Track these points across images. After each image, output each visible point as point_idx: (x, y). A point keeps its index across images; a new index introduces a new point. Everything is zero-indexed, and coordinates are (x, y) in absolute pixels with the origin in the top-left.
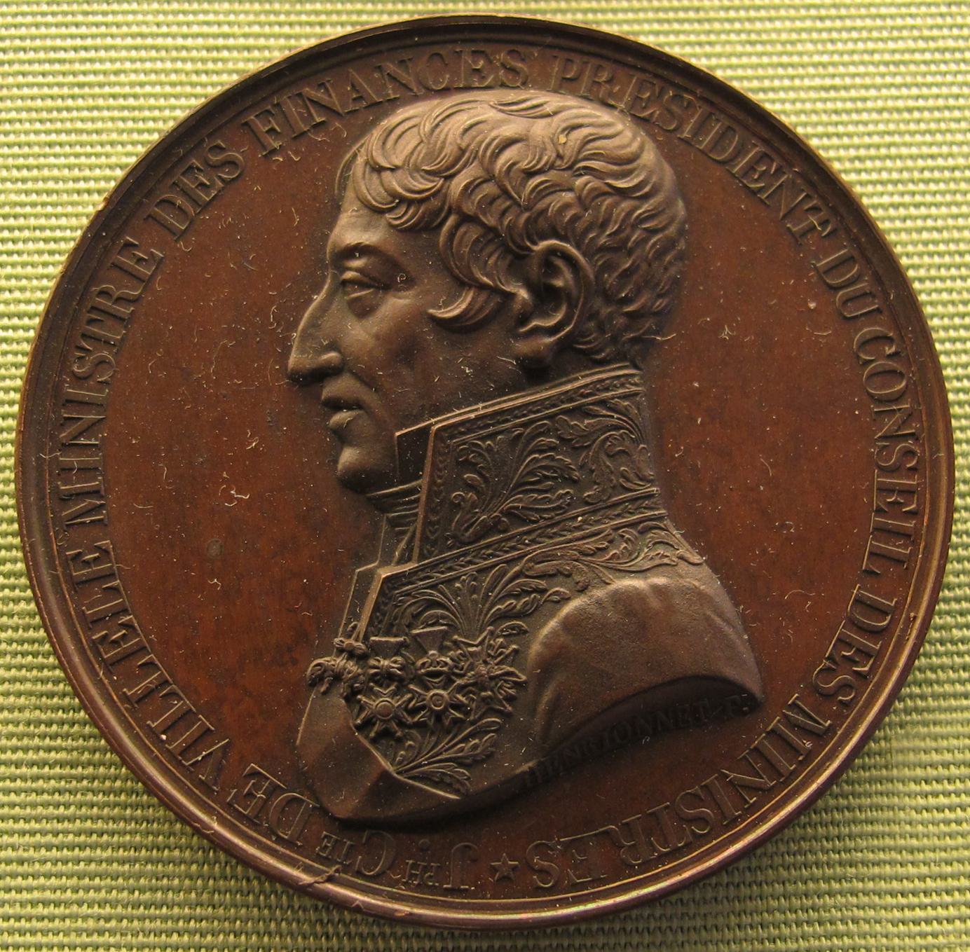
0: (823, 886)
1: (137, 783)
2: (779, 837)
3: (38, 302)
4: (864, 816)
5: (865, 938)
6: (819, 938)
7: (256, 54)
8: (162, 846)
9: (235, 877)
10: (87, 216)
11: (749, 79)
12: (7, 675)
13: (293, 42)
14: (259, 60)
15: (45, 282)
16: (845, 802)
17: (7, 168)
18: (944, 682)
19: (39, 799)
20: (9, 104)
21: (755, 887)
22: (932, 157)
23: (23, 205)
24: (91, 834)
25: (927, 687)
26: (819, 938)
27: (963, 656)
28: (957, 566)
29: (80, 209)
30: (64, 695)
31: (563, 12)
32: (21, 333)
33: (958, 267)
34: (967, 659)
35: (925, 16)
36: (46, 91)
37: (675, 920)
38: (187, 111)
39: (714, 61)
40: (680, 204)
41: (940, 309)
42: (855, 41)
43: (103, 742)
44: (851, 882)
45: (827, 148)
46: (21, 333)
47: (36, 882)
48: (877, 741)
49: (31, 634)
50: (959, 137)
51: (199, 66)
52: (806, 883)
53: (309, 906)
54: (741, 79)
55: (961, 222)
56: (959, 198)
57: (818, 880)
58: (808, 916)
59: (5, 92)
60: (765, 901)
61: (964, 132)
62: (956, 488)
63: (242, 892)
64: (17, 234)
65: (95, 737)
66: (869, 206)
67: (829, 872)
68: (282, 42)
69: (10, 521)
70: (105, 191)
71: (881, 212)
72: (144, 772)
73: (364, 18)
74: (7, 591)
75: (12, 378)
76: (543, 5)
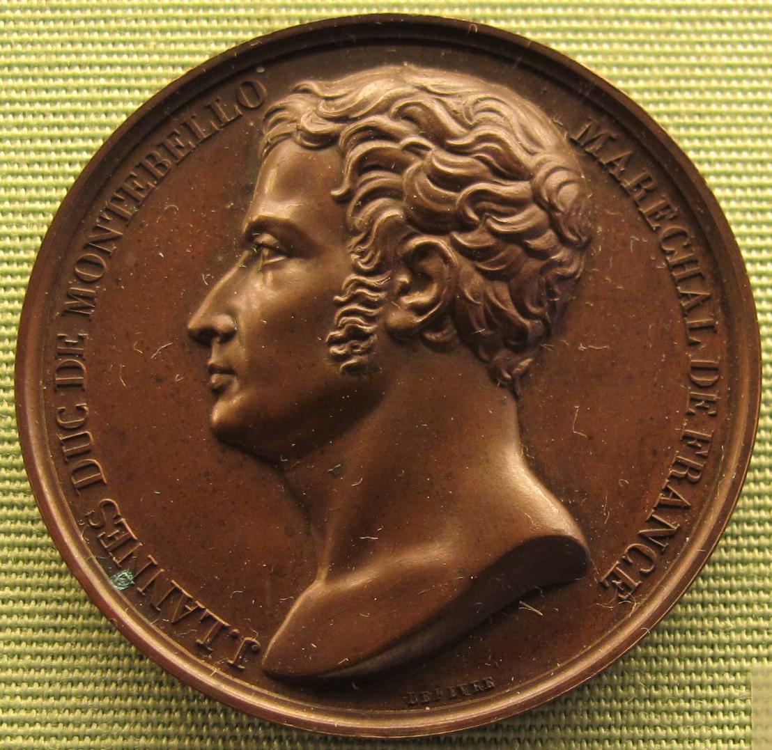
1: (130, 646)
4: (706, 584)
9: (216, 724)
10: (81, 163)
12: (7, 539)
19: (26, 607)
25: (720, 566)
29: (75, 156)
30: (70, 586)
31: (506, 19)
35: (688, 102)
43: (64, 565)
47: (32, 728)
48: (689, 591)
49: (17, 485)
53: (273, 736)
58: (611, 705)
59: (4, 132)
65: (56, 561)
66: (721, 199)
69: (763, 312)
72: (101, 599)
74: (7, 590)
75: (20, 262)
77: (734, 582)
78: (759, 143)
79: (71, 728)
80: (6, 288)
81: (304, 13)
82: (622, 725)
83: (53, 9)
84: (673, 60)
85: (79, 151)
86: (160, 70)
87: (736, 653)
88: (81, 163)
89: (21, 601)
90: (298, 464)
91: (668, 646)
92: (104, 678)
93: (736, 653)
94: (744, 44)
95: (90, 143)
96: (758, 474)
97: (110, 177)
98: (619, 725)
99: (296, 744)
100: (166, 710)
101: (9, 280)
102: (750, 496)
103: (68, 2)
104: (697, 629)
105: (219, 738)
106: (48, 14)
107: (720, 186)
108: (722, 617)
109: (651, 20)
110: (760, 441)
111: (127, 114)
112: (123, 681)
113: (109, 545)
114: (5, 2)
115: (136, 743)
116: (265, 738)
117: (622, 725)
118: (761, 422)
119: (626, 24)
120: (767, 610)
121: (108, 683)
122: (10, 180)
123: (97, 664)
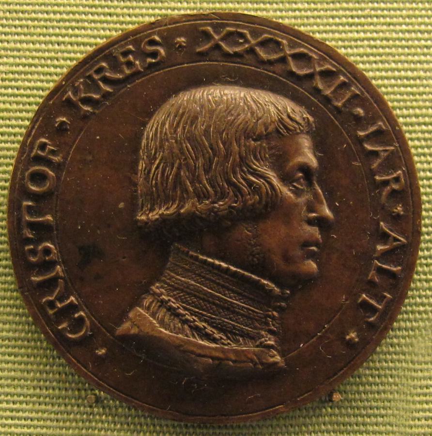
5: (391, 370)
7: (134, 19)
8: (83, 413)
13: (124, 26)
20: (5, 60)
22: (420, 62)
27: (426, 259)
28: (424, 261)
34: (430, 245)
40: (25, 294)
41: (417, 143)
44: (384, 386)
45: (368, 71)
51: (411, 12)
55: (426, 66)
56: (426, 20)
64: (366, 27)
67: (370, 412)
68: (118, 26)
73: (169, 12)
76: (243, 5)
77: (376, 396)
81: (164, 12)
82: (315, 424)
85: (75, 52)
87: (364, 405)
90: (274, 316)
91: (378, 385)
93: (364, 405)
95: (69, 62)
96: (405, 316)
98: (296, 432)
99: (163, 427)
102: (421, 265)
104: (382, 375)
107: (375, 78)
108: (376, 400)
109: (388, 78)
110: (417, 273)
113: (54, 296)
116: (138, 423)
117: (315, 424)
118: (418, 262)
119: (375, 20)
121: (48, 388)
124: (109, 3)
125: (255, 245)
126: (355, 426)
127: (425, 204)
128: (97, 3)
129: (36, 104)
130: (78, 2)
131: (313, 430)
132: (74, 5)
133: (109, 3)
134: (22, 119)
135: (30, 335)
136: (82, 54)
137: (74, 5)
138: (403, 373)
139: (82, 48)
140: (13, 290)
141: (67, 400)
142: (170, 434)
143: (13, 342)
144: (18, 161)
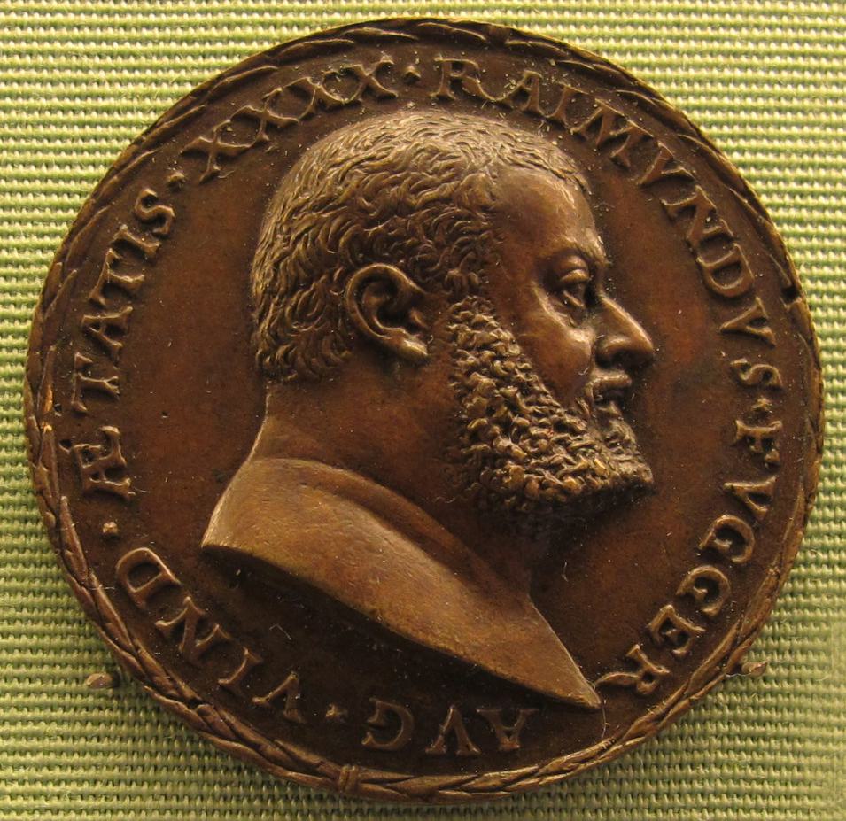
0: (697, 786)
2: (685, 717)
3: (23, 320)
6: (726, 811)
11: (650, 66)
14: (215, 68)
15: (91, 171)
16: (825, 557)
17: (8, 54)
18: (778, 665)
21: (698, 726)
23: (31, 179)
24: (65, 695)
26: (726, 811)
32: (25, 283)
33: (833, 209)
36: (813, 62)
37: (566, 786)
38: (119, 154)
39: (601, 43)
41: (830, 342)
42: (756, 42)
46: (25, 283)
50: (835, 145)
52: (691, 783)
54: (642, 66)
57: (741, 694)
60: (635, 800)
61: (839, 579)
62: (823, 370)
63: (174, 752)
70: (161, 109)
71: (715, 130)
78: (833, 201)
79: (89, 727)
80: (6, 277)
83: (562, 10)
84: (618, 30)
85: (102, 151)
86: (165, 88)
88: (105, 165)
89: (30, 621)
92: (119, 732)
94: (827, 111)
97: (119, 190)
100: (199, 768)
101: (10, 270)
102: (828, 492)
103: (429, 3)
104: (785, 649)
105: (268, 798)
106: (556, 15)
111: (147, 125)
112: (74, 621)
114: (9, 4)
115: (518, 395)
120: (840, 456)
122: (12, 46)
123: (85, 745)
124: (158, 5)
125: (308, 340)
126: (701, 768)
127: (825, 366)
128: (700, 5)
129: (75, 207)
130: (607, 4)
131: (635, 804)
132: (542, 9)
133: (124, 5)
134: (43, 249)
135: (80, 670)
136: (93, 182)
137: (542, 9)
138: (769, 658)
139: (212, 61)
140: (45, 548)
141: (158, 758)
142: (350, 815)
143: (51, 656)
144: (61, 256)
